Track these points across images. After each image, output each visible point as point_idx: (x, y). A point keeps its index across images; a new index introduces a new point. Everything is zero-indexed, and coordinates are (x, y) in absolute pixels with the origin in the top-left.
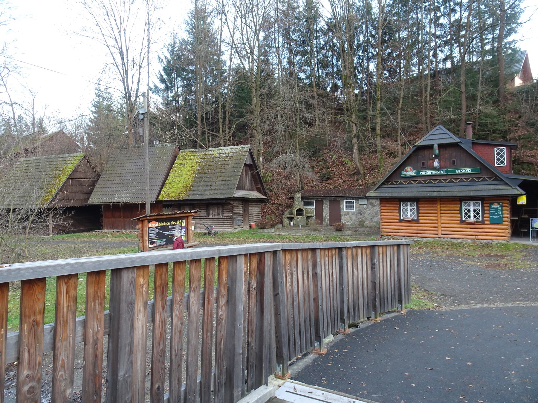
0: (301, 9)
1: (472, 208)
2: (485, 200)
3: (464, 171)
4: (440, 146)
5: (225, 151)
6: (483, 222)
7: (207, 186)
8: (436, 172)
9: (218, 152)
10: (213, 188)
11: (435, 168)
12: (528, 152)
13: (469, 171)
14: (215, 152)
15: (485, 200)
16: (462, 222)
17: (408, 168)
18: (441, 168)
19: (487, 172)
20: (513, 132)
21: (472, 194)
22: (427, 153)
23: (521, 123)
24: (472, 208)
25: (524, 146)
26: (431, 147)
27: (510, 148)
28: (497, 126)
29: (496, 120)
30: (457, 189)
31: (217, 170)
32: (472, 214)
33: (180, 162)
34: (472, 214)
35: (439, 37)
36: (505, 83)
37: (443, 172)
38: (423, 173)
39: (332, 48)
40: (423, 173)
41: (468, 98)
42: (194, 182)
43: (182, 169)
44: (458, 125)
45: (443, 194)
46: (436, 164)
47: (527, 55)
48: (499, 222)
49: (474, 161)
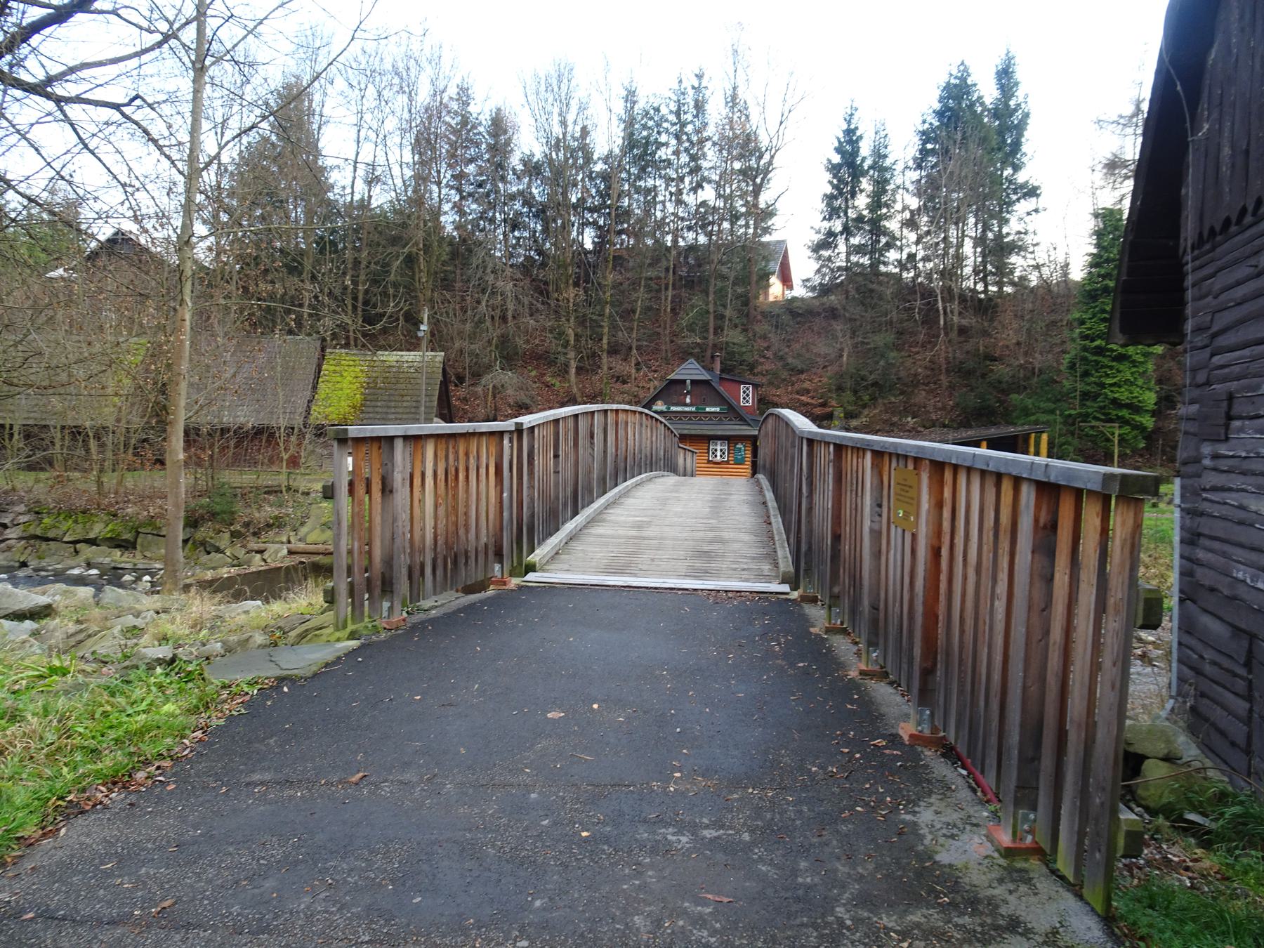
0: (481, 129)
1: (719, 448)
2: (731, 440)
3: (713, 410)
4: (693, 382)
5: (406, 358)
6: (727, 462)
7: (389, 407)
8: (687, 409)
9: (395, 358)
10: (400, 410)
11: (686, 405)
12: (774, 391)
13: (718, 409)
14: (391, 357)
15: (731, 440)
16: (709, 462)
17: (659, 402)
18: (691, 405)
19: (733, 412)
20: (761, 364)
21: (719, 433)
22: (678, 387)
23: (769, 354)
24: (719, 448)
25: (770, 383)
26: (684, 381)
27: (755, 386)
28: (745, 357)
29: (744, 349)
30: (706, 427)
31: (399, 386)
32: (719, 453)
33: (332, 368)
34: (719, 453)
35: (683, 219)
36: (757, 297)
37: (694, 409)
38: (673, 409)
39: (528, 201)
40: (673, 409)
41: (715, 317)
42: (365, 399)
43: (339, 379)
44: (704, 351)
45: (693, 432)
46: (688, 400)
47: (786, 257)
48: (740, 462)
49: (722, 400)
